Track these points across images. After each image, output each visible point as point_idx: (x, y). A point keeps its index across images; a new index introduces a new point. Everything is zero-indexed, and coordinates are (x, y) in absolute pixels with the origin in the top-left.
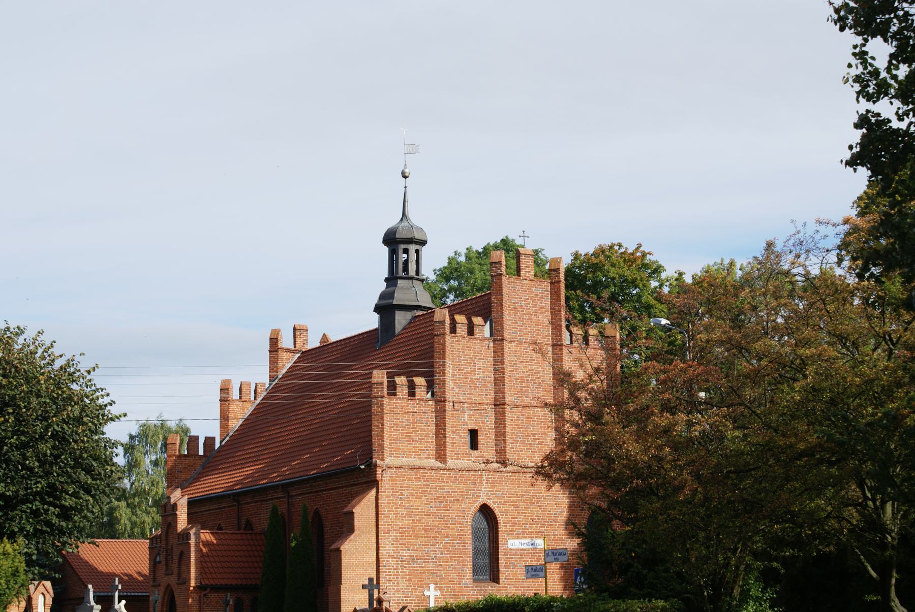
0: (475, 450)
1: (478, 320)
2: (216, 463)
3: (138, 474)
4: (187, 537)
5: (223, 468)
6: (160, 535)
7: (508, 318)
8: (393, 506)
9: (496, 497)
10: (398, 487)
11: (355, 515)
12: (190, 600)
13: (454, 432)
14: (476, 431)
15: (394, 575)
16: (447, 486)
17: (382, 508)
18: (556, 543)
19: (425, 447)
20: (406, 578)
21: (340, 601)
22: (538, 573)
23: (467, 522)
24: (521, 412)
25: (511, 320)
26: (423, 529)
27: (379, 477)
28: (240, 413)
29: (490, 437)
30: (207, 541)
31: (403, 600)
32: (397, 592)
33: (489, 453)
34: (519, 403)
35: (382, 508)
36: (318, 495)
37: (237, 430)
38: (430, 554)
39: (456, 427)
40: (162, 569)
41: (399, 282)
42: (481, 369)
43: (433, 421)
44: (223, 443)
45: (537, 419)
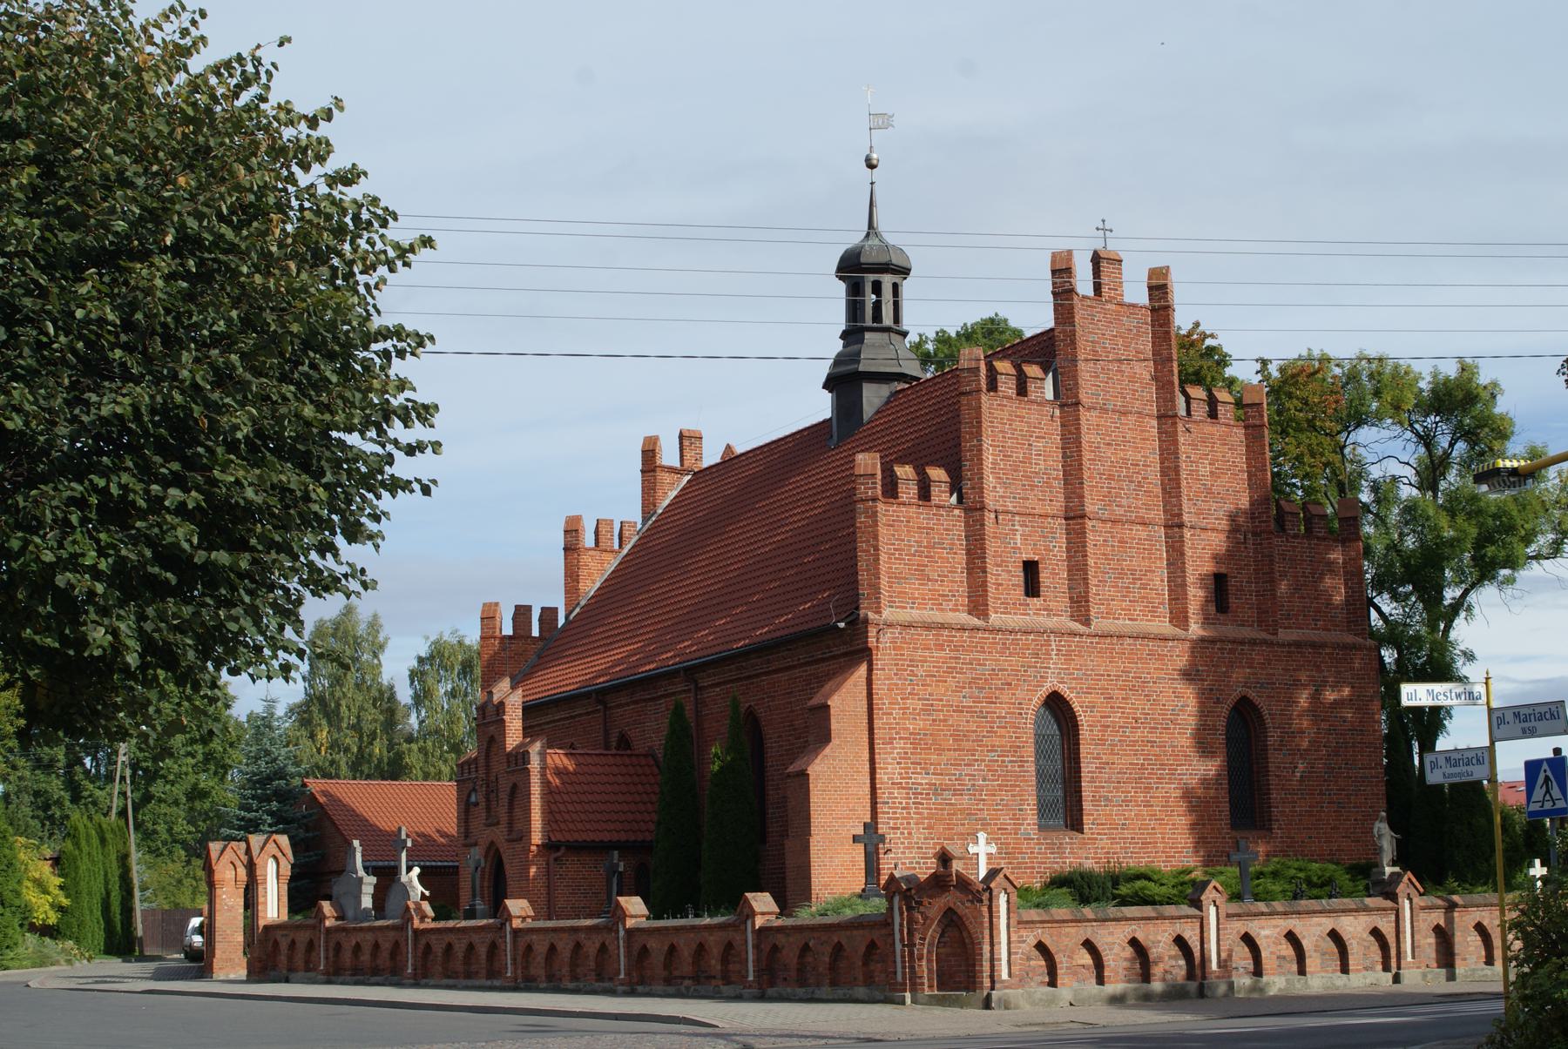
0: (1033, 596)
1: (1032, 370)
4: (524, 758)
6: (476, 758)
7: (1085, 370)
9: (1074, 679)
11: (832, 711)
12: (533, 870)
13: (998, 566)
14: (1036, 563)
16: (991, 660)
17: (880, 699)
18: (1176, 760)
19: (950, 591)
20: (923, 823)
22: (1470, 768)
23: (1025, 723)
24: (1110, 532)
25: (1088, 372)
26: (951, 736)
27: (872, 642)
28: (597, 573)
29: (1058, 574)
31: (918, 863)
32: (908, 848)
33: (1058, 602)
35: (880, 699)
36: (753, 683)
37: (593, 597)
38: (964, 780)
39: (1001, 556)
40: (480, 814)
41: (868, 335)
42: (1040, 455)
43: (961, 545)
44: (571, 617)
45: (1137, 544)
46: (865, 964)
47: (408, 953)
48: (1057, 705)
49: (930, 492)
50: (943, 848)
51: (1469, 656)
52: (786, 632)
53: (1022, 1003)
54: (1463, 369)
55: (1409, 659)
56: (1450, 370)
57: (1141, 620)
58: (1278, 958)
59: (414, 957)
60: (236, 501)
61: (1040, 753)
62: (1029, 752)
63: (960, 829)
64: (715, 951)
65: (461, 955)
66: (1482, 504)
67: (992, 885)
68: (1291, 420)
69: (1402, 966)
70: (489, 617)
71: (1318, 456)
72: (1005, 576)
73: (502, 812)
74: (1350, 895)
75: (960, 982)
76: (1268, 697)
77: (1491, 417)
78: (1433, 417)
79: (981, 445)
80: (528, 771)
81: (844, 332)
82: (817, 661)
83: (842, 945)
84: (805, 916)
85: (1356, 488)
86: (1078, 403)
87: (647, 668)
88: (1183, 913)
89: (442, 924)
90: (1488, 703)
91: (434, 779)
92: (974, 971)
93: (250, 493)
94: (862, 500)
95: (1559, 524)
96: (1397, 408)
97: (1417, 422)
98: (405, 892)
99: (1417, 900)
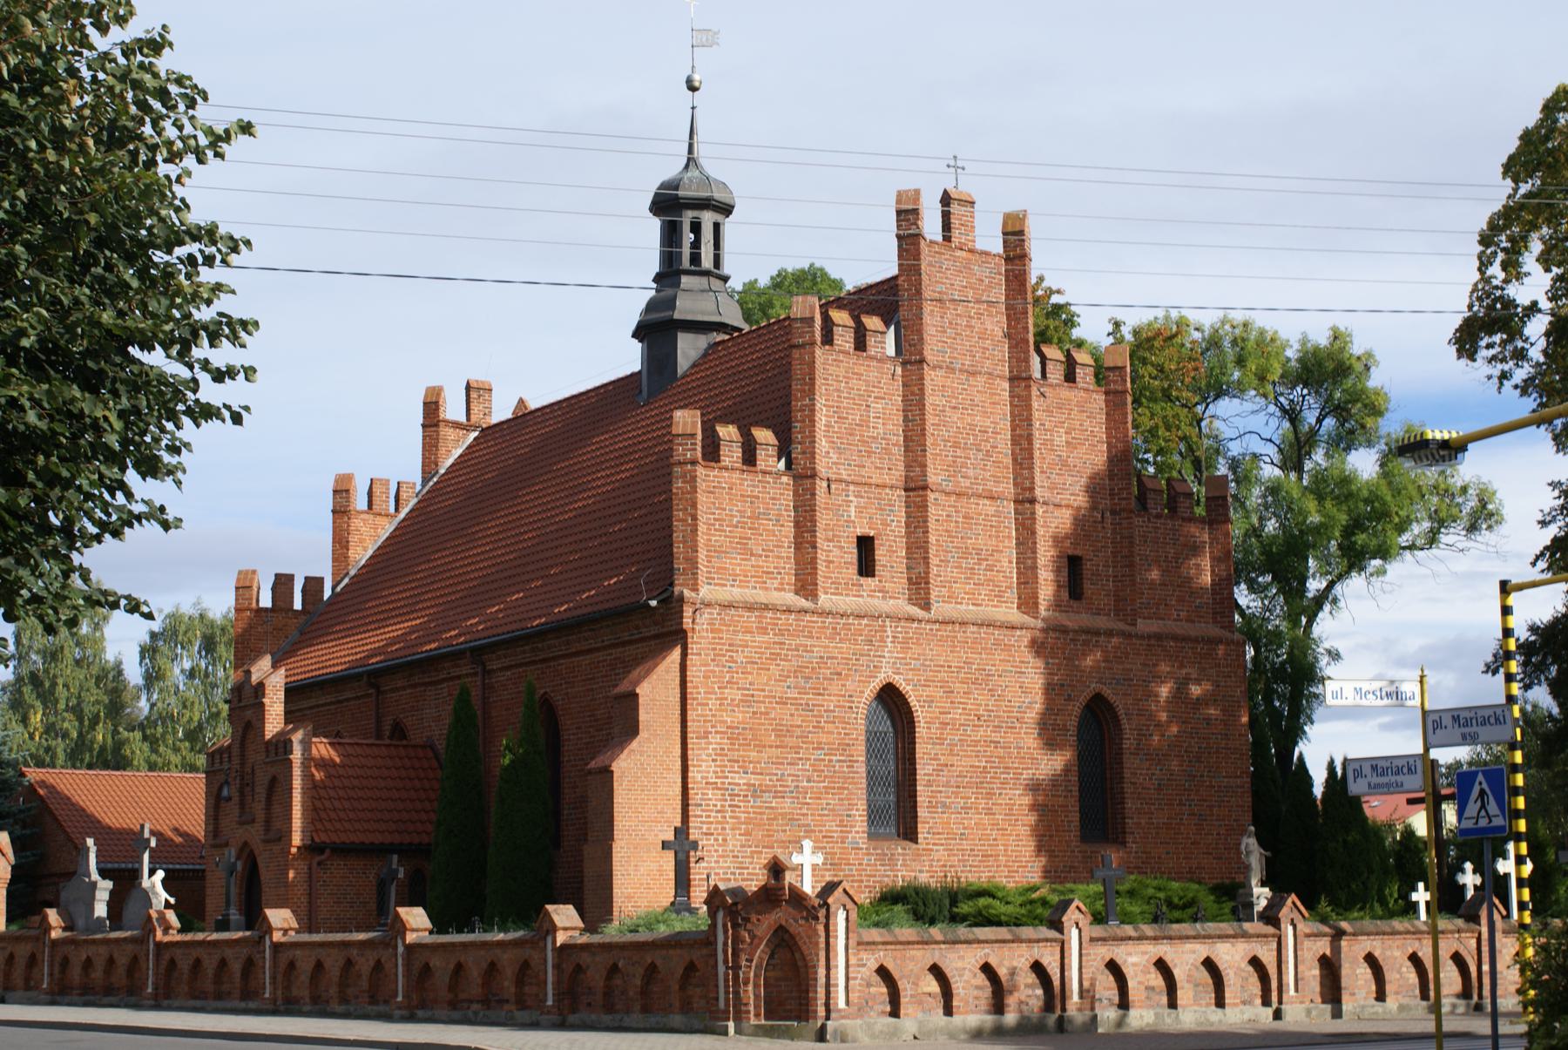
0: (867, 576)
1: (873, 322)
2: (326, 624)
3: (161, 691)
5: (340, 631)
6: (229, 746)
7: (931, 319)
8: (713, 683)
10: (724, 644)
11: (641, 700)
12: (291, 874)
13: (829, 541)
15: (717, 823)
21: (611, 875)
22: (1399, 778)
30: (322, 759)
31: (734, 874)
34: (950, 488)
37: (364, 566)
40: (232, 810)
41: (684, 279)
44: (338, 589)
46: (683, 988)
47: (148, 969)
48: (891, 700)
49: (755, 455)
50: (775, 857)
51: (1335, 655)
52: (589, 609)
53: (860, 1035)
54: (1336, 338)
55: (1267, 658)
56: (1322, 339)
57: (987, 605)
58: (1146, 988)
59: (156, 974)
60: (14, 428)
61: (872, 752)
62: (860, 752)
63: (782, 836)
64: (509, 972)
65: (210, 972)
66: (1353, 487)
67: (830, 901)
68: (1145, 388)
69: (1284, 1000)
70: (244, 587)
71: (1174, 430)
72: (836, 552)
73: (258, 808)
74: (1214, 919)
75: (791, 1011)
76: (1124, 694)
77: (1364, 391)
78: (1299, 389)
79: (814, 405)
80: (290, 762)
81: (657, 274)
82: (624, 644)
83: (655, 966)
84: (612, 932)
85: (1212, 465)
86: (922, 361)
87: (428, 648)
88: (1042, 936)
89: (189, 937)
90: (1422, 704)
91: (162, 769)
92: (807, 998)
93: (32, 417)
94: (680, 463)
95: (1436, 511)
96: (1262, 378)
97: (1282, 394)
98: (146, 899)
99: (1303, 927)
